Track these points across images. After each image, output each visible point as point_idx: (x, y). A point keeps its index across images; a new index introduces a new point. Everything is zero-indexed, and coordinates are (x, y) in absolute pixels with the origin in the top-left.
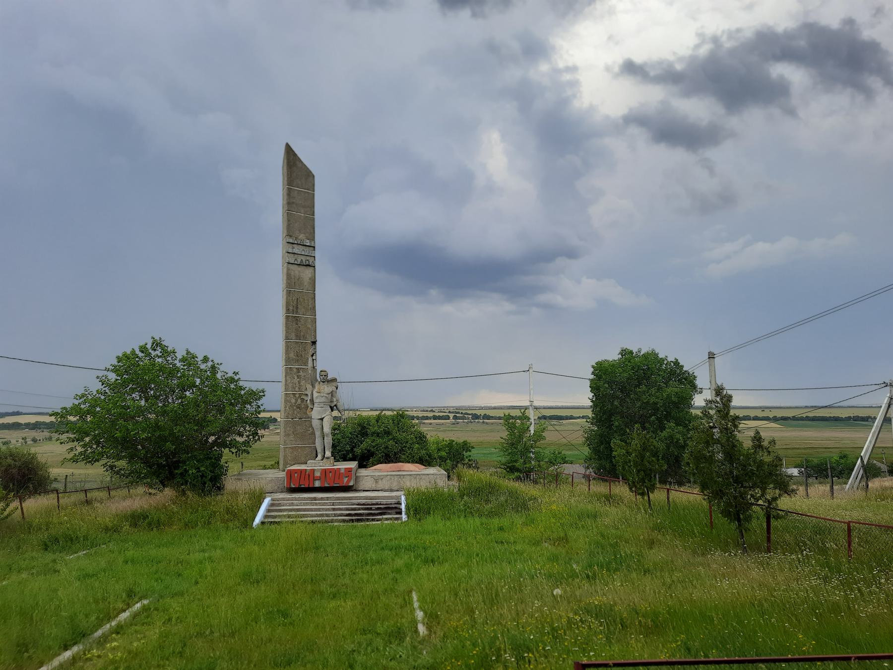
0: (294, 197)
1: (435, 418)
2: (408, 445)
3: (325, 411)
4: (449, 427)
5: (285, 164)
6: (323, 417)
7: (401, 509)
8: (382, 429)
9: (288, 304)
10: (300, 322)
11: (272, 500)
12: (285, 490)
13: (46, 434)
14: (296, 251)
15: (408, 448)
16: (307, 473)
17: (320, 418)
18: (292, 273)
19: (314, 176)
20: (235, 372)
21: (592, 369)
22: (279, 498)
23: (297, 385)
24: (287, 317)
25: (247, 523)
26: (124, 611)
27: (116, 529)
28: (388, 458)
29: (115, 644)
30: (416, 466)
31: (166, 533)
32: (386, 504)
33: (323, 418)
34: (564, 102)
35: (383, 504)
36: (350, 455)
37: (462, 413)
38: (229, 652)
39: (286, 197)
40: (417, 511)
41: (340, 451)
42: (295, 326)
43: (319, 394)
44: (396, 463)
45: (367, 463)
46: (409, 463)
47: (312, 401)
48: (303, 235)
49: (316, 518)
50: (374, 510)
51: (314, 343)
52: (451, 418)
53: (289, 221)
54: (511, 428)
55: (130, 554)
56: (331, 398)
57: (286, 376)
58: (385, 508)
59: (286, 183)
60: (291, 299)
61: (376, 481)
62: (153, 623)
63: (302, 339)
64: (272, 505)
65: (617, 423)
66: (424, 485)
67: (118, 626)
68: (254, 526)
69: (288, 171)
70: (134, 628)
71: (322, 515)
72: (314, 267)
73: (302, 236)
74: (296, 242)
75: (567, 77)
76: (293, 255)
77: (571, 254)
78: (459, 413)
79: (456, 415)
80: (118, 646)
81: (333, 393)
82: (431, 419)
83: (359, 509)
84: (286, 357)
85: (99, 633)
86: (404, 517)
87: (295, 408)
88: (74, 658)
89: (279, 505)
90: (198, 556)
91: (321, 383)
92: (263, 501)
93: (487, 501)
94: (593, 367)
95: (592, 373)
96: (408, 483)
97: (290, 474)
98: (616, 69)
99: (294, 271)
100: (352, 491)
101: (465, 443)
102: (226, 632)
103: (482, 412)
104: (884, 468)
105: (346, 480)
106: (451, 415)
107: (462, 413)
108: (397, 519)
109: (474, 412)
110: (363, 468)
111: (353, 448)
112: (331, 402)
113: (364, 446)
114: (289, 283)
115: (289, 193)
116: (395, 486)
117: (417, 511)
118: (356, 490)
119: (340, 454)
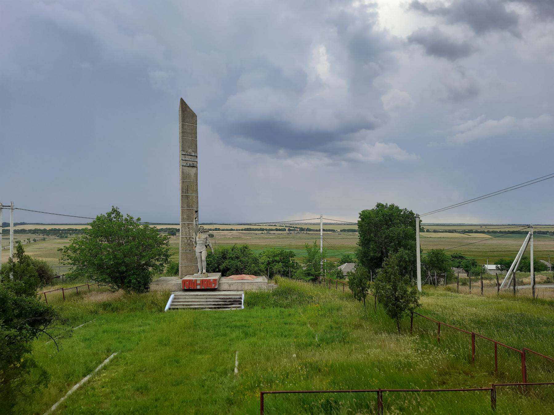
0: (186, 129)
1: (277, 230)
2: (248, 265)
3: (203, 248)
4: (285, 235)
5: (181, 109)
6: (201, 251)
7: (241, 302)
8: (234, 256)
9: (182, 189)
11: (175, 296)
13: (41, 236)
14: (187, 159)
15: (248, 266)
16: (193, 282)
18: (185, 171)
19: (196, 116)
21: (359, 215)
22: (178, 295)
23: (188, 232)
25: (161, 310)
26: (106, 359)
27: (96, 312)
28: (238, 272)
29: (104, 374)
31: (121, 314)
32: (234, 299)
34: (368, 27)
35: (232, 299)
37: (293, 227)
38: (153, 379)
39: (181, 129)
41: (211, 267)
42: (186, 200)
47: (196, 242)
48: (190, 150)
50: (227, 302)
51: (197, 212)
52: (287, 230)
53: (183, 142)
54: (309, 252)
55: (105, 327)
58: (234, 301)
59: (181, 120)
61: (230, 286)
62: (120, 365)
64: (175, 298)
65: (372, 246)
66: (254, 289)
67: (104, 366)
68: (165, 310)
69: (182, 114)
70: (111, 367)
72: (197, 167)
73: (190, 151)
74: (187, 154)
75: (371, 10)
77: (369, 127)
78: (292, 227)
79: (290, 228)
80: (106, 376)
82: (274, 231)
83: (220, 301)
84: (182, 218)
85: (97, 369)
86: (243, 307)
87: (187, 245)
88: (89, 381)
89: (178, 299)
90: (138, 329)
91: (200, 233)
92: (170, 297)
93: (287, 298)
94: (360, 214)
95: (360, 217)
96: (247, 287)
97: (184, 282)
100: (217, 291)
102: (152, 370)
104: (549, 265)
105: (213, 285)
106: (287, 229)
107: (293, 227)
112: (206, 243)
113: (224, 265)
114: (183, 177)
115: (183, 126)
116: (239, 288)
119: (211, 269)
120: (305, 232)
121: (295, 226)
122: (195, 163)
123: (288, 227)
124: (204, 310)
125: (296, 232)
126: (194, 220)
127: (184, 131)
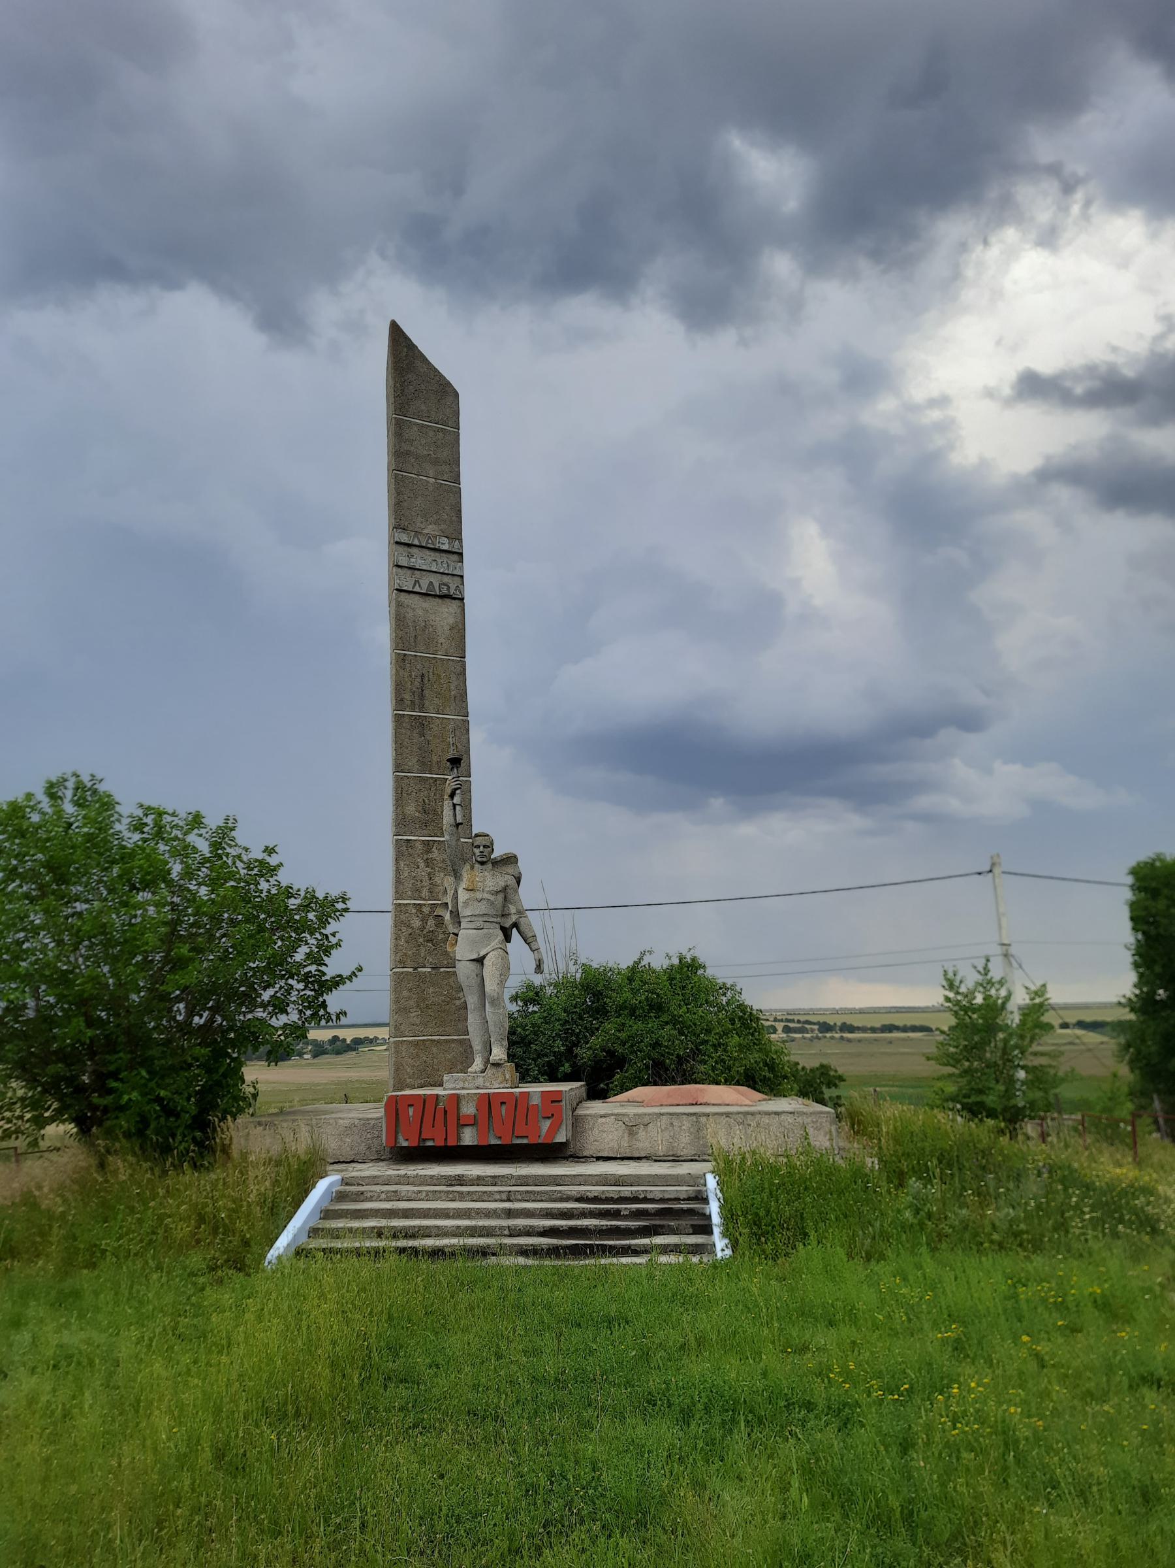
3: (489, 937)
6: (482, 953)
7: (709, 1217)
10: (430, 729)
11: (345, 1182)
12: (387, 1155)
14: (417, 562)
17: (475, 956)
18: (410, 615)
19: (456, 395)
20: (267, 848)
23: (426, 883)
24: (398, 719)
30: (739, 1092)
32: (662, 1200)
33: (484, 957)
35: (652, 1201)
36: (567, 1065)
37: (799, 1021)
40: (759, 1227)
41: (540, 1055)
42: (417, 738)
43: (472, 894)
44: (683, 1083)
45: (607, 1085)
46: (718, 1083)
49: (454, 1241)
50: (626, 1218)
51: (455, 762)
53: (399, 494)
56: (504, 907)
57: (397, 861)
59: (392, 408)
60: (406, 675)
61: (631, 1130)
63: (435, 769)
64: (341, 1197)
69: (396, 382)
71: (474, 1232)
72: (462, 599)
74: (416, 542)
75: (935, 415)
76: (409, 572)
78: (793, 1021)
81: (508, 890)
83: (583, 1214)
86: (720, 1242)
87: (421, 940)
91: (477, 865)
96: (722, 1137)
98: (1007, 391)
99: (414, 609)
100: (566, 1158)
101: (824, 1070)
103: (838, 1020)
108: (697, 1249)
109: (822, 1019)
110: (599, 1099)
111: (572, 1047)
115: (398, 430)
116: (684, 1143)
117: (759, 1227)
118: (577, 1158)
120: (837, 1036)
121: (802, 1018)
122: (453, 583)
123: (782, 1021)
124: (493, 1260)
125: (808, 1036)
126: (447, 804)
127: (406, 447)
